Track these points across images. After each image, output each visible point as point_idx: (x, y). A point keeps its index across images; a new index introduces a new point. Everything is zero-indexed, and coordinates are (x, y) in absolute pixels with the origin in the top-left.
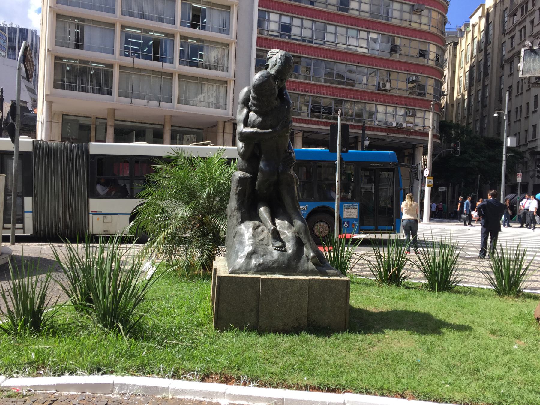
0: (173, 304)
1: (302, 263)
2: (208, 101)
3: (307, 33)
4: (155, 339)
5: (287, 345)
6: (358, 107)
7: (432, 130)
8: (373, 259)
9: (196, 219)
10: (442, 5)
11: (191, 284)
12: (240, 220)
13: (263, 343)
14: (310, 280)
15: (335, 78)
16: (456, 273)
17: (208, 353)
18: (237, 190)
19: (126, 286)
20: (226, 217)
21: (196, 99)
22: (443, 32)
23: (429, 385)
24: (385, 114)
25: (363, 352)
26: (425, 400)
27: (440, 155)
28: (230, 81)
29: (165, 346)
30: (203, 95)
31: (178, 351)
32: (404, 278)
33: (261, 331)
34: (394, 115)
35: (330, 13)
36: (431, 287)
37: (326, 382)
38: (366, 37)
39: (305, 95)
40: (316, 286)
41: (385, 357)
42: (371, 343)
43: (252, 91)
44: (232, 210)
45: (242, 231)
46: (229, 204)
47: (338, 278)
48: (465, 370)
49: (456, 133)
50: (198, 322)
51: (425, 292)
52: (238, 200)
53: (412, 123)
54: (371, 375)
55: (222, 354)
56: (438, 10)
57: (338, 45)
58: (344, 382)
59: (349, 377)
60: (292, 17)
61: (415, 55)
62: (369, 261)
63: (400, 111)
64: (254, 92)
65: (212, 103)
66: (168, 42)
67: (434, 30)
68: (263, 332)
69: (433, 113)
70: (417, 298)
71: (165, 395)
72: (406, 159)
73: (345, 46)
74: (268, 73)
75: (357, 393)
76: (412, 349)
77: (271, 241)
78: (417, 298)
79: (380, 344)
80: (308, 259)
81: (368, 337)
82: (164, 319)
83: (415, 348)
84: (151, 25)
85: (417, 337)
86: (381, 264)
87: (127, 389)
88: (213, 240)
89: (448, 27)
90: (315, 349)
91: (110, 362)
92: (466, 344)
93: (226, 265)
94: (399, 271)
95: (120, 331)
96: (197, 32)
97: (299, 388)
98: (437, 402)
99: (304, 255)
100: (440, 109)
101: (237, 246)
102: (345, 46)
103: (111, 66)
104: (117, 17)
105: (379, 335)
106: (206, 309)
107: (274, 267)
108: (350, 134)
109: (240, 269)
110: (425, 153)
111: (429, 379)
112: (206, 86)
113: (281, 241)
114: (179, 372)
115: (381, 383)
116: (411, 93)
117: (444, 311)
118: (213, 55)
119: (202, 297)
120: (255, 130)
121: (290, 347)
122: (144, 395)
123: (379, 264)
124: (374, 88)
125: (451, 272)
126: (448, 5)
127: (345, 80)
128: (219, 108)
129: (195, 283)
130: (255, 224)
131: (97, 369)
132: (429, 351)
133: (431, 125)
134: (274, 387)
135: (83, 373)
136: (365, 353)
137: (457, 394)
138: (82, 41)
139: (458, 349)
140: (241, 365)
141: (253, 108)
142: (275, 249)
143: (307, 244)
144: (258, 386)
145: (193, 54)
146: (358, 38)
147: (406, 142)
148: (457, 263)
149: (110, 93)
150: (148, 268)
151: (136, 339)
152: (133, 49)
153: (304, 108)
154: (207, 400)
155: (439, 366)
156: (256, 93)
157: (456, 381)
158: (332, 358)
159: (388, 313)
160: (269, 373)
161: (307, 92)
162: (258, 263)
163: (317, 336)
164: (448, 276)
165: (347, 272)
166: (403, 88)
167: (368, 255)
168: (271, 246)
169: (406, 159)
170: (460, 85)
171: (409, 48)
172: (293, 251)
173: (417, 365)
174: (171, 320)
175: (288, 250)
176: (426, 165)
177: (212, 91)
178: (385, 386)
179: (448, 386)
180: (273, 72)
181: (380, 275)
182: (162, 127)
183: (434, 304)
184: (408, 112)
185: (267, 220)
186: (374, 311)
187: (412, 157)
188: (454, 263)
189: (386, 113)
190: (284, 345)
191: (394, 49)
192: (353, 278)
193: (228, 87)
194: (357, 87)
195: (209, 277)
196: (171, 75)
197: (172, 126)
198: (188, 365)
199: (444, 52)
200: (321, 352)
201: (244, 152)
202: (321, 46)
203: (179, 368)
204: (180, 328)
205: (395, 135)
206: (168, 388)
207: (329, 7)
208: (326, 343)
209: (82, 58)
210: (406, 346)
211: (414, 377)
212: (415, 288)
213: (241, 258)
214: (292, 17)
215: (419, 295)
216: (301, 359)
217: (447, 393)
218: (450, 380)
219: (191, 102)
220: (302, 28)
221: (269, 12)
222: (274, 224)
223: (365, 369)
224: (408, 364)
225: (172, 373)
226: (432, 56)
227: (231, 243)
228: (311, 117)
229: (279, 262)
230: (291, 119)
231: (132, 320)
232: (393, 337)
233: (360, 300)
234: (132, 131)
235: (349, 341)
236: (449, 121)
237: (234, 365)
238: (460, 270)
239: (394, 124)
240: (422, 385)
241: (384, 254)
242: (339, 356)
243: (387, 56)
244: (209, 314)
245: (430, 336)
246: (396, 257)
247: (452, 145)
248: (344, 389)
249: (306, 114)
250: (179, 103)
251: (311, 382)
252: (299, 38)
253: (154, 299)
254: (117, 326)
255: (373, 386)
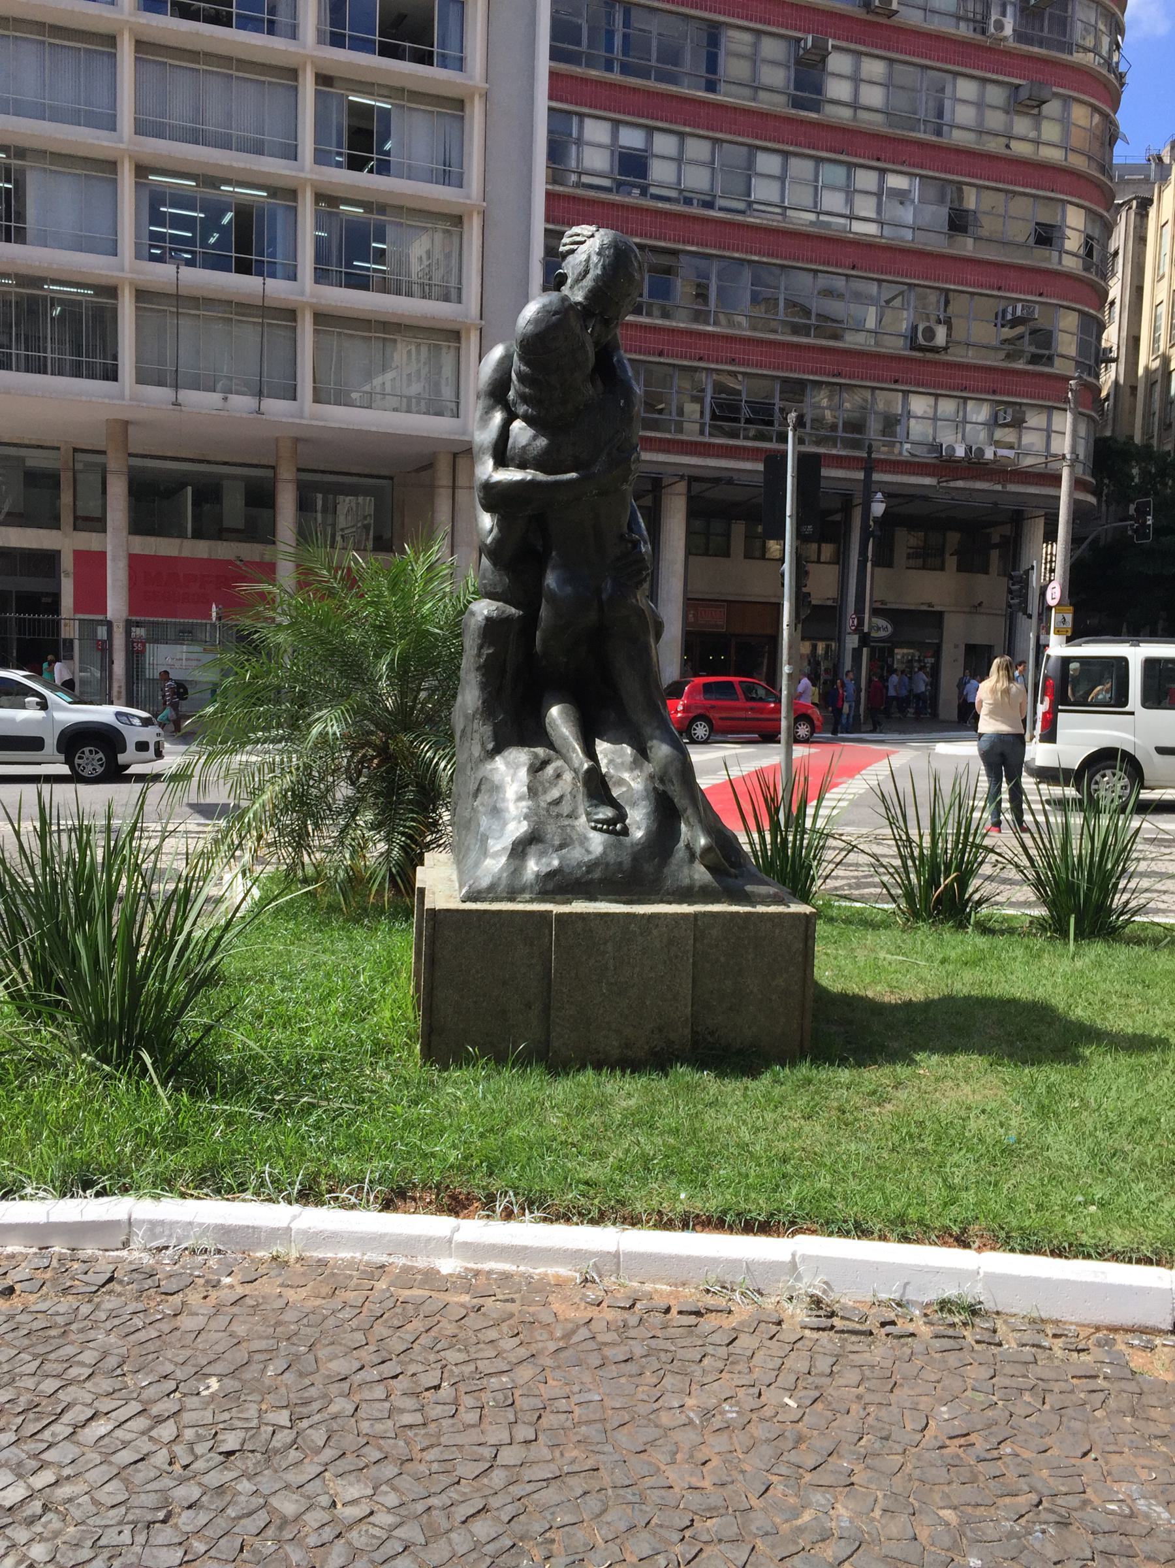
0: (304, 991)
1: (673, 867)
2: (406, 392)
3: (697, 179)
4: (249, 1092)
5: (632, 1102)
6: (850, 402)
7: (1071, 466)
8: (886, 851)
9: (369, 744)
10: (1105, 85)
11: (359, 934)
12: (490, 746)
13: (561, 1097)
14: (696, 915)
15: (781, 316)
16: (1132, 885)
17: (403, 1128)
18: (479, 655)
19: (162, 944)
20: (452, 736)
21: (367, 388)
22: (1105, 167)
23: (1040, 1207)
24: (935, 422)
25: (851, 1118)
26: (1025, 1251)
27: (1096, 540)
28: (468, 331)
29: (278, 1111)
30: (389, 375)
31: (317, 1127)
32: (979, 903)
33: (556, 1062)
34: (960, 423)
35: (763, 115)
36: (1055, 927)
37: (743, 1205)
38: (873, 187)
39: (696, 369)
40: (714, 932)
41: (914, 1130)
42: (874, 1092)
43: (516, 358)
44: (466, 716)
45: (496, 778)
46: (459, 698)
47: (781, 909)
48: (1145, 1164)
49: (1144, 473)
50: (376, 1042)
51: (1039, 942)
52: (484, 686)
53: (1012, 448)
54: (873, 1182)
55: (442, 1132)
56: (1092, 101)
57: (789, 213)
58: (795, 1205)
59: (807, 1189)
60: (650, 130)
61: (1021, 239)
62: (873, 856)
63: (978, 413)
64: (521, 358)
65: (418, 398)
66: (280, 216)
67: (1078, 162)
68: (564, 1068)
69: (1073, 414)
70: (1015, 959)
71: (278, 1249)
72: (995, 554)
73: (812, 217)
74: (565, 299)
75: (831, 1234)
76: (994, 1104)
77: (582, 806)
78: (1015, 959)
79: (902, 1094)
80: (692, 857)
81: (866, 1074)
82: (278, 1035)
83: (1004, 1104)
84: (226, 163)
85: (1007, 1072)
86: (910, 863)
87: (170, 1236)
88: (411, 802)
89: (1121, 154)
90: (712, 1112)
91: (120, 1161)
92: (1150, 1088)
93: (455, 877)
94: (963, 882)
95: (144, 1070)
96: (365, 180)
97: (664, 1223)
98: (1060, 1256)
99: (681, 844)
100: (1098, 403)
101: (484, 821)
102: (812, 217)
103: (111, 291)
104: (302, 170)
105: (898, 1068)
106: (397, 1005)
107: (591, 881)
108: (823, 484)
109: (492, 887)
110: (1050, 536)
111: (1039, 1191)
112: (399, 346)
113: (613, 803)
114: (319, 1184)
115: (899, 1205)
116: (1009, 357)
117: (1090, 995)
118: (418, 251)
119: (387, 971)
120: (527, 475)
121: (640, 1109)
122: (219, 1252)
123: (905, 866)
124: (901, 342)
125: (1116, 885)
126: (1122, 85)
127: (813, 321)
128: (439, 413)
129: (370, 929)
130: (536, 756)
131: (80, 1180)
132: (1043, 1112)
133: (1067, 450)
134: (593, 1222)
135: (41, 1194)
136: (856, 1120)
137: (1119, 1231)
138: (21, 217)
139: (1129, 1103)
140: (498, 1162)
141: (522, 409)
142: (595, 828)
143: (689, 812)
144: (545, 1220)
145: (352, 250)
146: (850, 192)
147: (996, 504)
148: (1134, 855)
149: (111, 374)
150: (233, 887)
151: (195, 1094)
152: (174, 238)
153: (692, 409)
154: (401, 1261)
155: (1070, 1153)
156: (527, 364)
157: (1118, 1194)
158: (763, 1136)
159: (928, 1005)
160: (579, 1182)
161: (701, 359)
162: (545, 870)
163: (721, 1074)
164: (1106, 897)
165: (814, 889)
166: (985, 342)
167: (878, 840)
168: (583, 819)
169: (995, 554)
170: (1156, 329)
171: (1005, 216)
172: (648, 833)
173: (1007, 1151)
174: (296, 1037)
175: (632, 830)
176: (1052, 571)
177: (418, 361)
178: (912, 1214)
179: (1093, 1209)
180: (578, 296)
181: (909, 895)
182: (269, 473)
183: (1064, 976)
184: (1001, 414)
185: (570, 744)
186: (886, 999)
187: (1012, 549)
188: (1124, 854)
189: (935, 419)
190: (624, 1104)
191: (959, 222)
192: (831, 906)
193: (463, 352)
194: (853, 340)
195: (408, 914)
196: (290, 314)
197: (299, 470)
198: (344, 1165)
199: (1108, 229)
200: (730, 1119)
201: (498, 541)
202: (740, 218)
203: (319, 1173)
204: (322, 1060)
205: (960, 484)
206: (289, 1229)
207: (762, 95)
208: (745, 1096)
209: (23, 271)
210: (978, 1097)
211: (996, 1185)
212: (1011, 931)
213: (496, 855)
214: (650, 130)
215: (1019, 952)
216: (672, 1141)
217: (1090, 1230)
218: (1099, 1192)
219: (354, 395)
220: (681, 165)
221: (581, 116)
222: (591, 753)
223: (855, 1166)
224: (982, 1149)
225: (297, 1187)
226: (1073, 242)
227: (467, 814)
228: (711, 435)
229: (607, 864)
230: (635, 440)
231: (184, 1037)
232: (941, 1072)
233: (849, 967)
234: (183, 486)
235: (812, 1088)
236: (1122, 439)
237: (476, 1161)
238: (1143, 875)
239: (960, 452)
240: (1018, 1209)
241: (921, 837)
242: (782, 1130)
243: (938, 243)
244: (407, 1019)
245: (1046, 1068)
246: (957, 842)
247: (1132, 508)
248: (793, 1223)
249: (697, 427)
250: (317, 400)
251: (700, 1205)
252: (673, 194)
253: (249, 979)
254: (139, 1058)
255: (877, 1213)
